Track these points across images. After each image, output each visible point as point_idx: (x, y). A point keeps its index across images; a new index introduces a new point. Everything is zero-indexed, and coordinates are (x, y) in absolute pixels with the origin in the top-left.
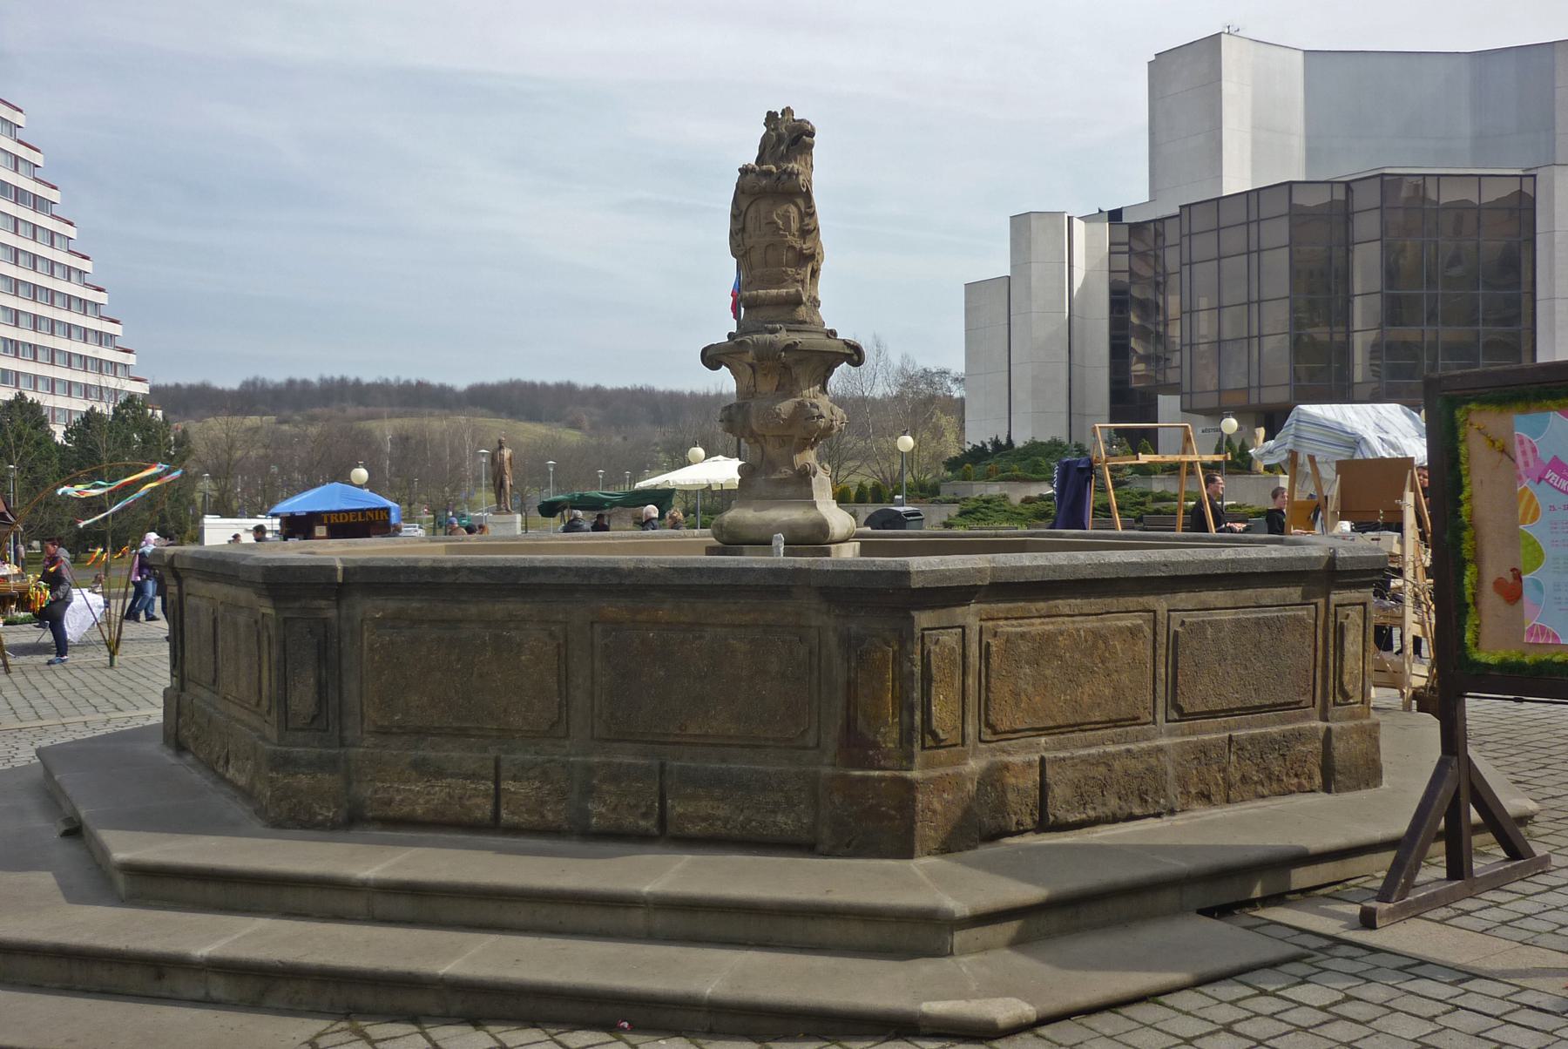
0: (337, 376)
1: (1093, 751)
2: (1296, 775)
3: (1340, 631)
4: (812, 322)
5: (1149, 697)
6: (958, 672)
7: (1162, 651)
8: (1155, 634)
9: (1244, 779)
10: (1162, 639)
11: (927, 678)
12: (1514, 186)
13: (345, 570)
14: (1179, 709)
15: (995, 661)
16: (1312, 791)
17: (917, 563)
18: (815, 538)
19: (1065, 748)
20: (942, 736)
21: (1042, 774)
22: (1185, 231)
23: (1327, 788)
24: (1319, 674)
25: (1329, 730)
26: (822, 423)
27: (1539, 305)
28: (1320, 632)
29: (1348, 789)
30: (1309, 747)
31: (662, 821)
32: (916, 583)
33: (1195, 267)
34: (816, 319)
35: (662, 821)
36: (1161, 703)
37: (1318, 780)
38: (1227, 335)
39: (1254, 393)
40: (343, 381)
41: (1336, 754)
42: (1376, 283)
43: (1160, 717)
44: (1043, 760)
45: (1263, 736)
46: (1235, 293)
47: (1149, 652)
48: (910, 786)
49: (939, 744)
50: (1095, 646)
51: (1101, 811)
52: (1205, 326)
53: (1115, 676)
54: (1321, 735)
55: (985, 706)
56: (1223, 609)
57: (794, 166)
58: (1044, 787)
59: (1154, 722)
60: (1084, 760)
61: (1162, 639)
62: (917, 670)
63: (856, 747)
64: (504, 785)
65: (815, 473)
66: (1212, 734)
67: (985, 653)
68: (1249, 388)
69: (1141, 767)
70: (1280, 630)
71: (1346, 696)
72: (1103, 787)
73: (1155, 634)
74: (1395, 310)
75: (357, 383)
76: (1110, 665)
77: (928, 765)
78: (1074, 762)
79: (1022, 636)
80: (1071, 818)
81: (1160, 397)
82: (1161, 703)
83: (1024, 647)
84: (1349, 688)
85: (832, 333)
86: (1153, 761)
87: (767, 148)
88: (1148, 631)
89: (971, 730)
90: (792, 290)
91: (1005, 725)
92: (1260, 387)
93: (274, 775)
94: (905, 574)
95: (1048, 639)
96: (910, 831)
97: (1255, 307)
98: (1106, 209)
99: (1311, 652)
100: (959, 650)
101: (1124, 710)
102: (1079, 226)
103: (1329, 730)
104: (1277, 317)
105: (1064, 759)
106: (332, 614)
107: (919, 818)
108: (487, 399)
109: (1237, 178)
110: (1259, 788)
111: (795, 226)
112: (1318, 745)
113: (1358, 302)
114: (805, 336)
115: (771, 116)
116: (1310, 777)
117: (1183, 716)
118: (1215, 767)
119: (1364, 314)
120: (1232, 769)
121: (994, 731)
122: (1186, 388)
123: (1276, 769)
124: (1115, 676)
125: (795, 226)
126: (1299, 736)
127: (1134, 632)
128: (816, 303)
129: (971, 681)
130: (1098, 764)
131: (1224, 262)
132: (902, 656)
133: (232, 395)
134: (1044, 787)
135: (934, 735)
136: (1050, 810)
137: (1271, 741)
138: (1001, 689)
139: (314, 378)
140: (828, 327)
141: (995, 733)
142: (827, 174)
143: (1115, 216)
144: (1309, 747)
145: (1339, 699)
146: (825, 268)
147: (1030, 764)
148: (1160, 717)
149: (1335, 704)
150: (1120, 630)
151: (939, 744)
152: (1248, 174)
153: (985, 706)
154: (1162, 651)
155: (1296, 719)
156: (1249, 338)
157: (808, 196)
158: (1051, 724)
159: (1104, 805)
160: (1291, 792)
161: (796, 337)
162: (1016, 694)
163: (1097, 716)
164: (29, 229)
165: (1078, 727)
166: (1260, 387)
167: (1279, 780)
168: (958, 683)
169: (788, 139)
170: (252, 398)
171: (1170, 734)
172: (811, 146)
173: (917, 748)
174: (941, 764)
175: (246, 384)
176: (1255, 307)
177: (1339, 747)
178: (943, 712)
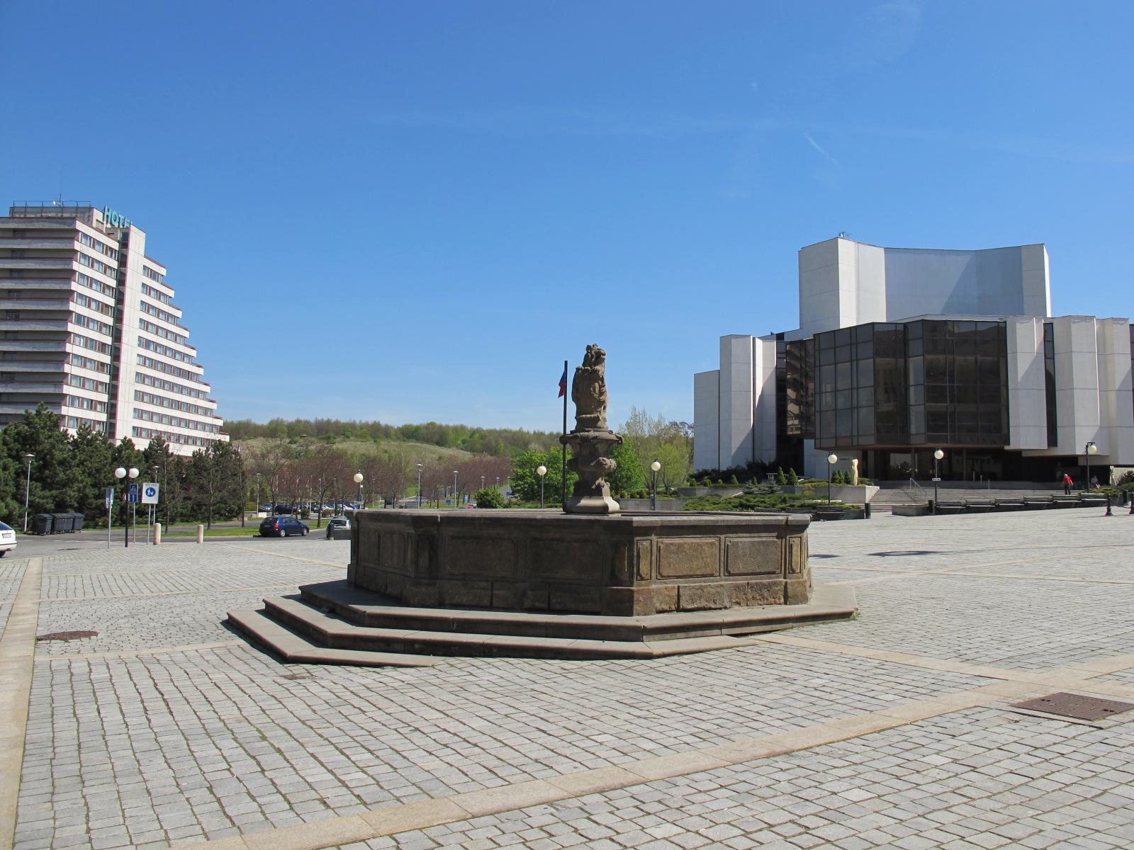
0: (325, 419)
1: (697, 584)
2: (774, 598)
3: (791, 547)
4: (603, 428)
5: (718, 567)
6: (649, 556)
7: (722, 552)
8: (720, 545)
9: (754, 598)
10: (723, 547)
11: (639, 556)
12: (996, 324)
13: (441, 517)
14: (729, 572)
15: (662, 552)
16: (780, 604)
17: (635, 518)
18: (604, 510)
19: (687, 583)
20: (643, 576)
21: (678, 592)
22: (817, 348)
23: (786, 603)
24: (783, 561)
25: (786, 582)
26: (606, 467)
27: (1010, 392)
28: (783, 547)
29: (794, 604)
30: (779, 588)
31: (549, 604)
32: (634, 525)
33: (823, 368)
34: (605, 426)
35: (549, 604)
36: (722, 569)
37: (782, 600)
38: (839, 406)
39: (855, 439)
40: (328, 422)
41: (789, 590)
42: (921, 380)
43: (722, 574)
44: (679, 587)
45: (761, 583)
46: (843, 384)
47: (718, 551)
48: (632, 591)
49: (642, 579)
50: (698, 549)
51: (701, 605)
52: (828, 399)
53: (705, 559)
54: (784, 584)
55: (658, 567)
56: (745, 539)
57: (598, 367)
58: (679, 596)
59: (720, 576)
60: (693, 587)
61: (723, 547)
62: (635, 553)
63: (615, 579)
64: (494, 592)
65: (603, 487)
66: (741, 581)
67: (659, 549)
68: (852, 436)
69: (714, 591)
70: (768, 545)
71: (794, 572)
72: (700, 597)
73: (720, 545)
74: (934, 393)
75: (337, 423)
76: (703, 555)
77: (638, 585)
78: (691, 588)
79: (672, 544)
80: (689, 607)
81: (805, 441)
82: (722, 569)
83: (672, 548)
84: (794, 567)
85: (611, 432)
86: (719, 589)
87: (587, 361)
88: (717, 543)
89: (653, 574)
90: (596, 415)
91: (665, 574)
92: (858, 436)
93: (413, 588)
94: (631, 522)
95: (681, 545)
96: (633, 612)
97: (855, 391)
98: (776, 332)
99: (780, 553)
100: (649, 548)
101: (708, 571)
102: (759, 343)
103: (786, 582)
104: (866, 396)
105: (686, 587)
106: (435, 532)
107: (635, 603)
108: (410, 434)
109: (848, 319)
110: (759, 602)
111: (597, 390)
112: (783, 588)
113: (912, 389)
114: (600, 433)
115: (589, 348)
116: (779, 599)
117: (730, 575)
118: (742, 593)
119: (916, 396)
120: (749, 594)
121: (662, 577)
122: (818, 436)
123: (766, 595)
124: (705, 559)
125: (597, 390)
126: (775, 584)
127: (712, 544)
128: (605, 420)
129: (654, 558)
130: (698, 589)
131: (839, 365)
132: (631, 550)
133: (261, 427)
134: (679, 596)
135: (641, 576)
136: (681, 604)
137: (764, 586)
138: (664, 562)
139: (312, 420)
140: (609, 429)
141: (662, 577)
142: (607, 370)
143: (780, 337)
144: (779, 588)
145: (791, 572)
146: (607, 408)
147: (674, 588)
148: (722, 574)
149: (789, 573)
150: (707, 543)
151: (642, 579)
152: (854, 315)
153: (658, 567)
154: (722, 552)
155: (774, 578)
156: (852, 408)
157: (602, 380)
158: (682, 574)
159: (700, 603)
160: (772, 604)
161: (597, 434)
162: (669, 563)
163: (698, 572)
164: (154, 329)
165: (691, 576)
166: (858, 436)
167: (767, 599)
168: (649, 559)
169: (594, 357)
170: (273, 431)
171: (726, 580)
172: (604, 359)
173: (635, 579)
174: (643, 586)
175: (271, 422)
176: (855, 391)
177: (790, 588)
178: (644, 568)
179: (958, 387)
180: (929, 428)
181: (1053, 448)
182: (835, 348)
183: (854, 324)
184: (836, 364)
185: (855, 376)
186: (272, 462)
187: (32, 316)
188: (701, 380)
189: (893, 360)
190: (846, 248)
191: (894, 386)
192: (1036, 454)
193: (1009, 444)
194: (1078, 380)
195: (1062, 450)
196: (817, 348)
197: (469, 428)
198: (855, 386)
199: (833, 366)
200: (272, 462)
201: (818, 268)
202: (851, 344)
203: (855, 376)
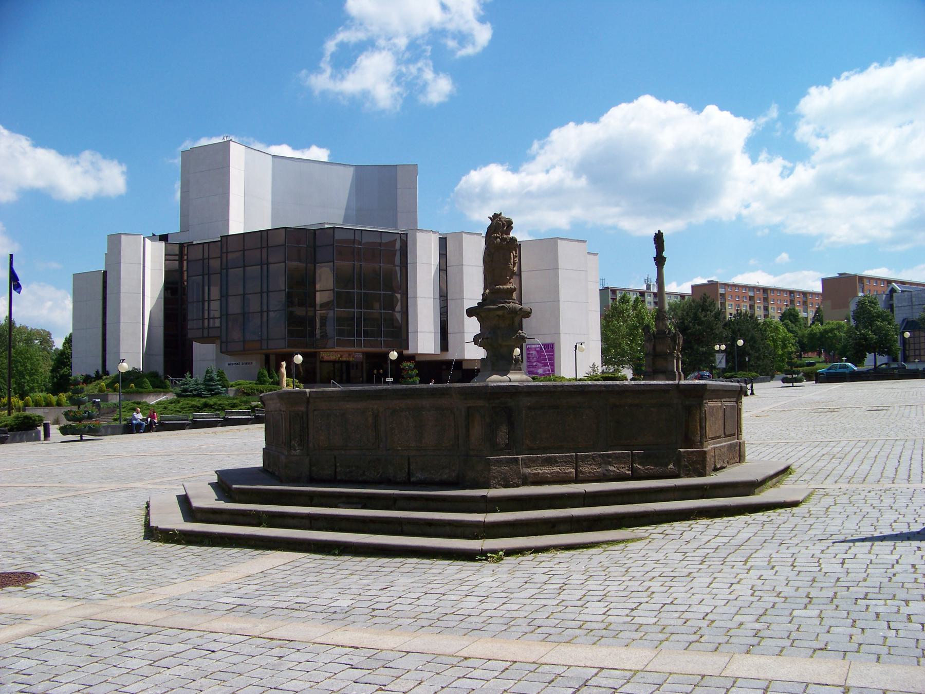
109: (236, 226)
131: (248, 269)
152: (242, 225)
179: (365, 293)
180: (291, 333)
181: (444, 353)
182: (244, 250)
183: (268, 226)
184: (244, 267)
185: (265, 281)
186: (384, 94)
187: (291, 521)
188: (80, 282)
189: (304, 265)
190: (237, 153)
191: (301, 288)
192: (428, 359)
193: (408, 349)
194: (420, 292)
195: (453, 355)
196: (225, 250)
197: (18, 326)
198: (265, 289)
199: (242, 269)
200: (384, 94)
201: (206, 174)
202: (262, 248)
203: (265, 281)
